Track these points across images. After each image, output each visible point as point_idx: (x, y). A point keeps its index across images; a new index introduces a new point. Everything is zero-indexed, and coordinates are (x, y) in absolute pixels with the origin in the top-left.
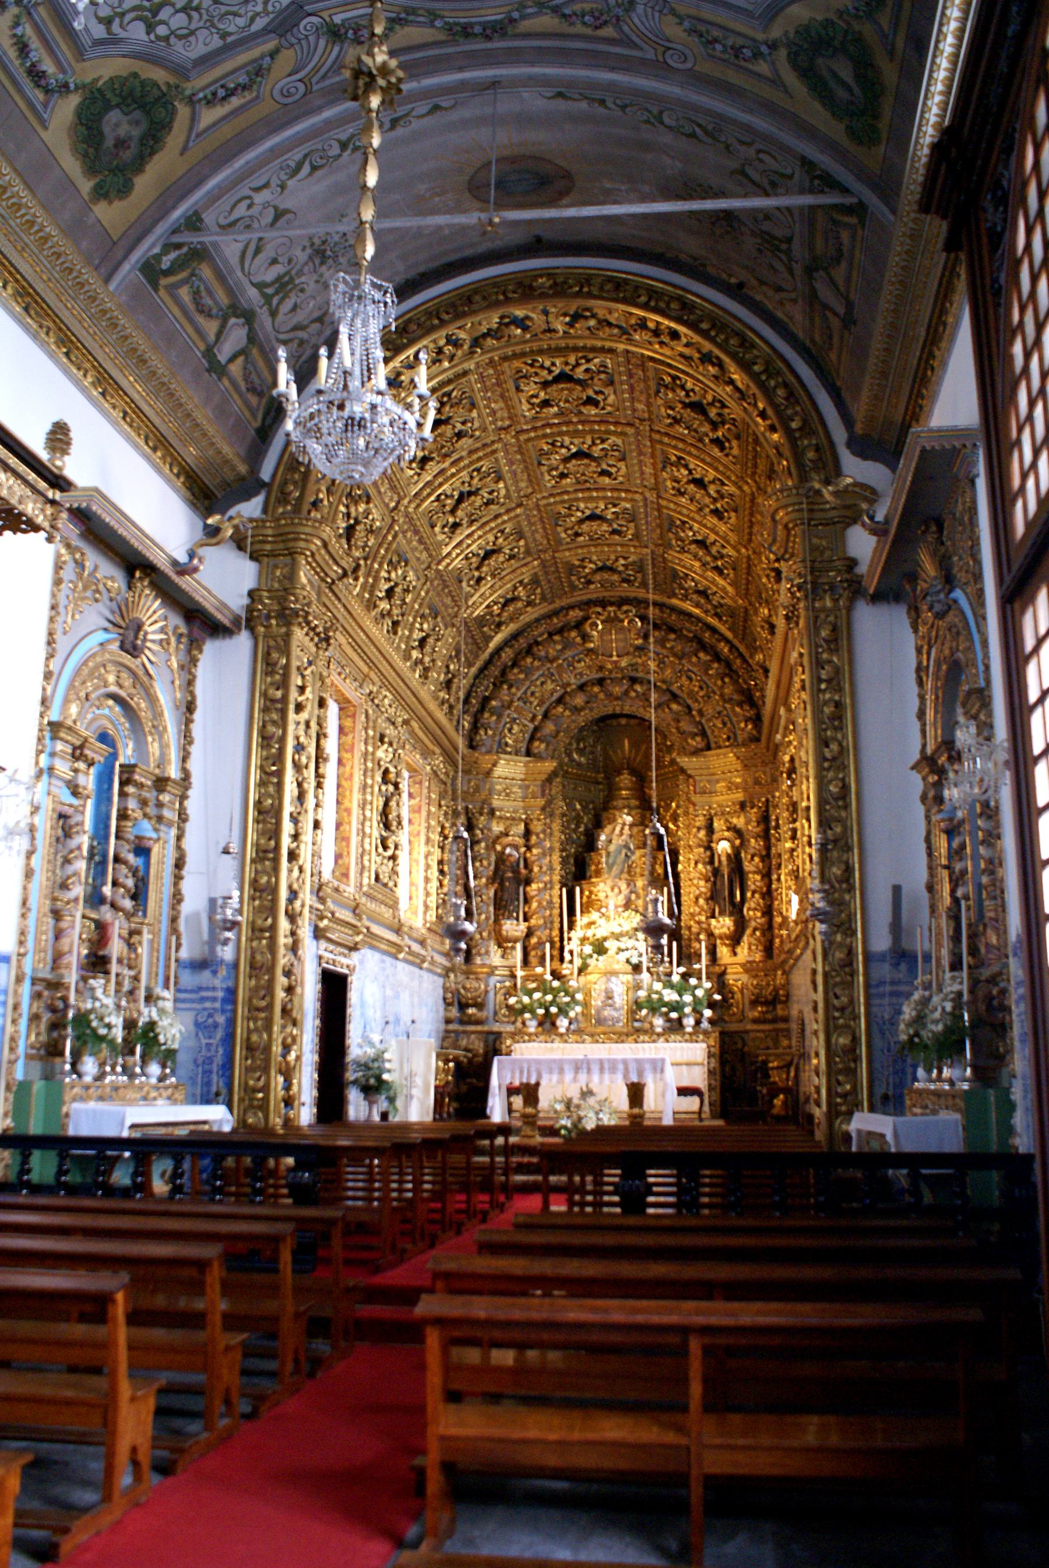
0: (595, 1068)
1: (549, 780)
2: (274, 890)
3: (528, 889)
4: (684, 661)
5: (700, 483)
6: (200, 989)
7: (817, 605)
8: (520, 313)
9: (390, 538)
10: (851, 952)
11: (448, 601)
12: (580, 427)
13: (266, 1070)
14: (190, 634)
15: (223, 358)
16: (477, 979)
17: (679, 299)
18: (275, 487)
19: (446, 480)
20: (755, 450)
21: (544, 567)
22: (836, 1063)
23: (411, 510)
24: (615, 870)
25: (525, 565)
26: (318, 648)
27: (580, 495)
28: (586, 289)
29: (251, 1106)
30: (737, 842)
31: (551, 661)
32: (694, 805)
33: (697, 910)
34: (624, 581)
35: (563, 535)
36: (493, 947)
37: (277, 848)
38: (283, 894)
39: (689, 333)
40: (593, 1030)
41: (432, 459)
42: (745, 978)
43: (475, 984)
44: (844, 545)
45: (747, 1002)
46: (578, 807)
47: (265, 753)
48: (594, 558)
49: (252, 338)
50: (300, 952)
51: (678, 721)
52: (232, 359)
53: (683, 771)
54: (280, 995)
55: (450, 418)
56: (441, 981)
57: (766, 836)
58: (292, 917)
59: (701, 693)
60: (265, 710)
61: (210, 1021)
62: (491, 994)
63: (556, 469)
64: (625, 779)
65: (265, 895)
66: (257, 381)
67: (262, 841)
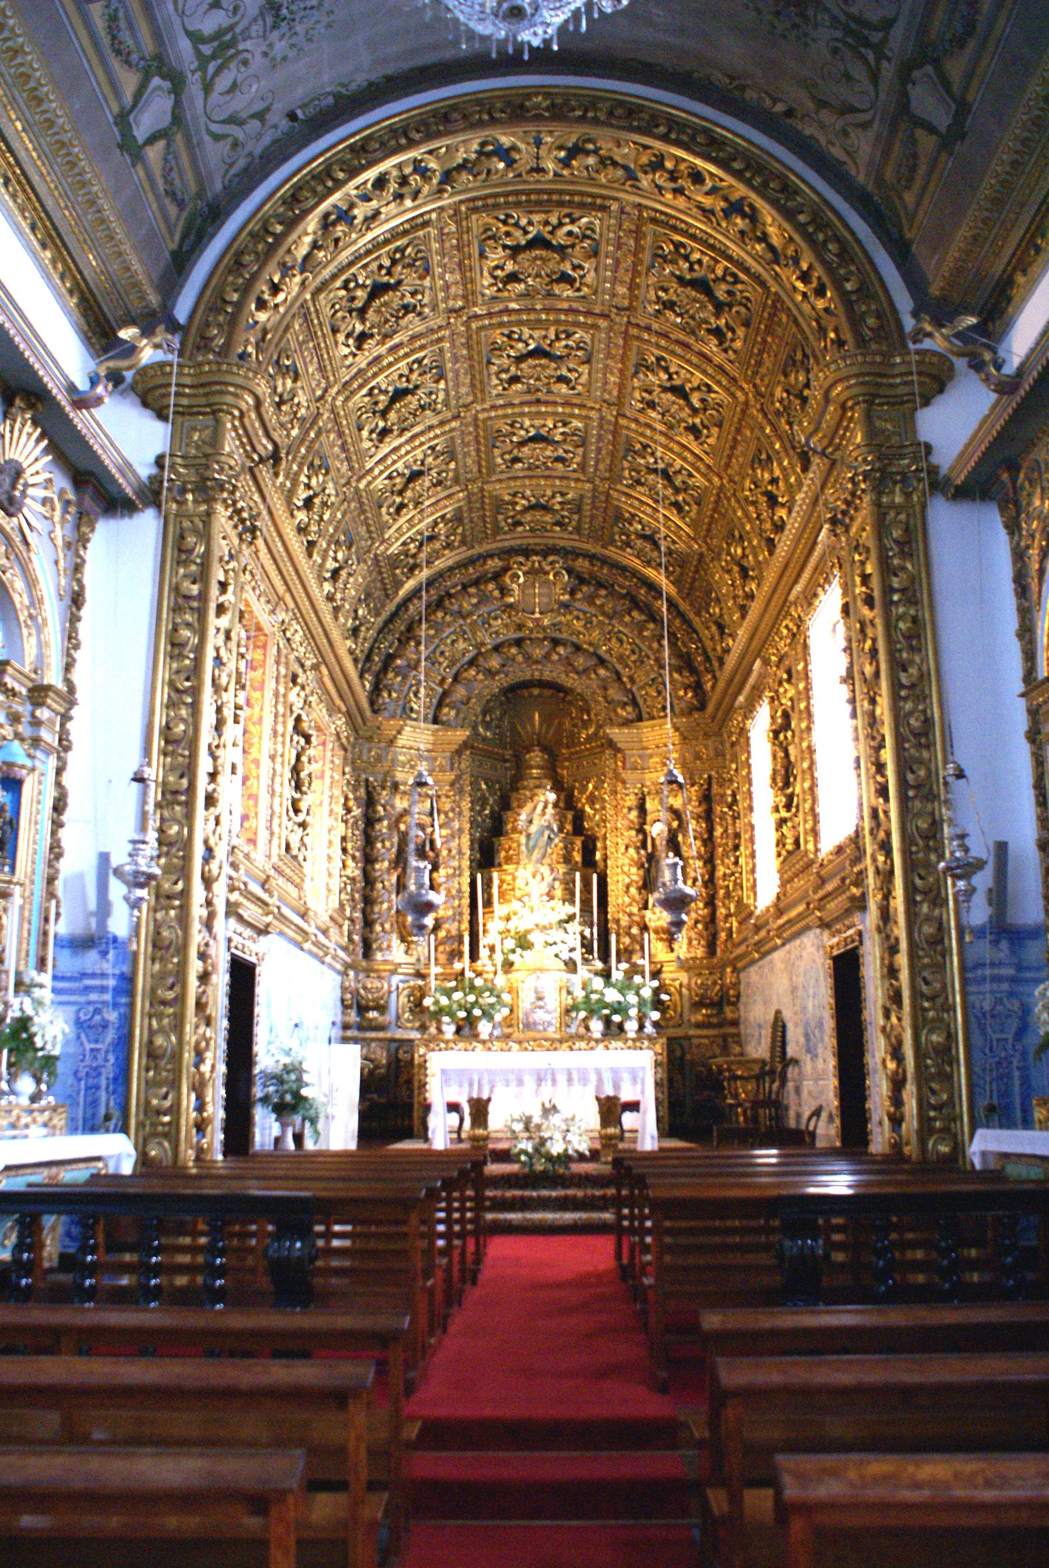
0: (562, 1078)
1: (459, 752)
2: (187, 845)
3: (435, 875)
4: (614, 622)
5: (680, 392)
6: (83, 975)
7: (885, 500)
8: (506, 141)
9: (312, 435)
10: (941, 928)
11: (362, 530)
12: (544, 317)
13: (175, 1084)
14: (80, 503)
15: (141, 133)
16: (379, 978)
17: (706, 131)
18: (193, 330)
19: (382, 370)
20: (764, 341)
21: (470, 502)
22: (927, 1067)
23: (339, 403)
24: (537, 854)
25: (449, 496)
26: (241, 540)
27: (526, 410)
28: (590, 114)
29: (155, 1135)
30: (675, 824)
31: (464, 618)
32: (624, 782)
33: (627, 900)
34: (558, 524)
35: (499, 461)
36: (395, 941)
37: (191, 789)
38: (198, 851)
39: (720, 173)
40: (521, 1036)
41: (372, 336)
42: (683, 977)
43: (377, 984)
44: (914, 431)
45: (687, 1005)
46: (484, 787)
47: (175, 665)
48: (528, 493)
49: (177, 118)
50: (214, 930)
51: (605, 689)
52: (152, 140)
53: (611, 744)
54: (193, 982)
55: (399, 283)
56: (339, 978)
57: (708, 816)
58: (208, 882)
59: (633, 658)
60: (176, 609)
61: (97, 1018)
62: (394, 996)
63: (507, 371)
64: (536, 757)
65: (174, 850)
66: (177, 183)
67: (171, 779)
